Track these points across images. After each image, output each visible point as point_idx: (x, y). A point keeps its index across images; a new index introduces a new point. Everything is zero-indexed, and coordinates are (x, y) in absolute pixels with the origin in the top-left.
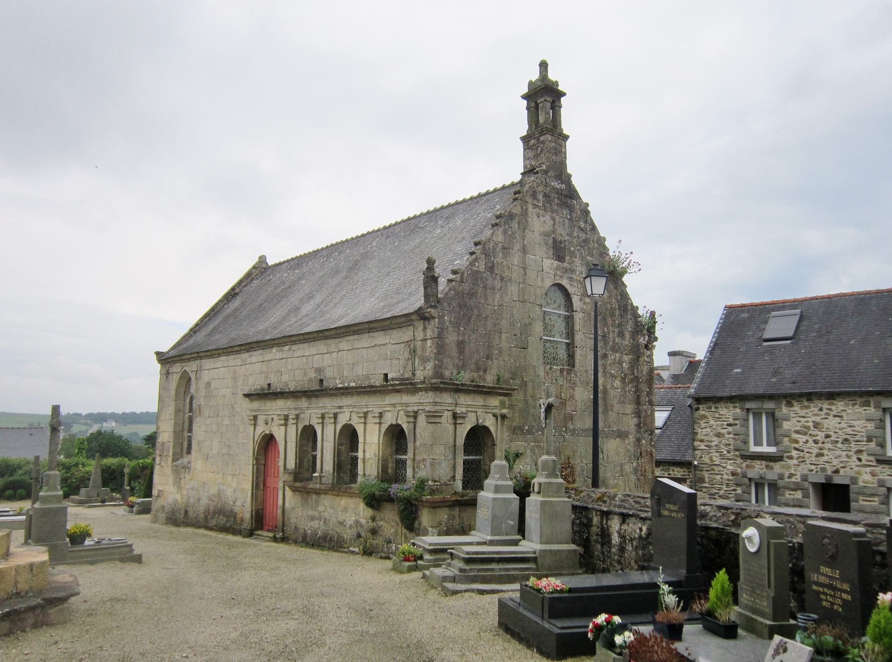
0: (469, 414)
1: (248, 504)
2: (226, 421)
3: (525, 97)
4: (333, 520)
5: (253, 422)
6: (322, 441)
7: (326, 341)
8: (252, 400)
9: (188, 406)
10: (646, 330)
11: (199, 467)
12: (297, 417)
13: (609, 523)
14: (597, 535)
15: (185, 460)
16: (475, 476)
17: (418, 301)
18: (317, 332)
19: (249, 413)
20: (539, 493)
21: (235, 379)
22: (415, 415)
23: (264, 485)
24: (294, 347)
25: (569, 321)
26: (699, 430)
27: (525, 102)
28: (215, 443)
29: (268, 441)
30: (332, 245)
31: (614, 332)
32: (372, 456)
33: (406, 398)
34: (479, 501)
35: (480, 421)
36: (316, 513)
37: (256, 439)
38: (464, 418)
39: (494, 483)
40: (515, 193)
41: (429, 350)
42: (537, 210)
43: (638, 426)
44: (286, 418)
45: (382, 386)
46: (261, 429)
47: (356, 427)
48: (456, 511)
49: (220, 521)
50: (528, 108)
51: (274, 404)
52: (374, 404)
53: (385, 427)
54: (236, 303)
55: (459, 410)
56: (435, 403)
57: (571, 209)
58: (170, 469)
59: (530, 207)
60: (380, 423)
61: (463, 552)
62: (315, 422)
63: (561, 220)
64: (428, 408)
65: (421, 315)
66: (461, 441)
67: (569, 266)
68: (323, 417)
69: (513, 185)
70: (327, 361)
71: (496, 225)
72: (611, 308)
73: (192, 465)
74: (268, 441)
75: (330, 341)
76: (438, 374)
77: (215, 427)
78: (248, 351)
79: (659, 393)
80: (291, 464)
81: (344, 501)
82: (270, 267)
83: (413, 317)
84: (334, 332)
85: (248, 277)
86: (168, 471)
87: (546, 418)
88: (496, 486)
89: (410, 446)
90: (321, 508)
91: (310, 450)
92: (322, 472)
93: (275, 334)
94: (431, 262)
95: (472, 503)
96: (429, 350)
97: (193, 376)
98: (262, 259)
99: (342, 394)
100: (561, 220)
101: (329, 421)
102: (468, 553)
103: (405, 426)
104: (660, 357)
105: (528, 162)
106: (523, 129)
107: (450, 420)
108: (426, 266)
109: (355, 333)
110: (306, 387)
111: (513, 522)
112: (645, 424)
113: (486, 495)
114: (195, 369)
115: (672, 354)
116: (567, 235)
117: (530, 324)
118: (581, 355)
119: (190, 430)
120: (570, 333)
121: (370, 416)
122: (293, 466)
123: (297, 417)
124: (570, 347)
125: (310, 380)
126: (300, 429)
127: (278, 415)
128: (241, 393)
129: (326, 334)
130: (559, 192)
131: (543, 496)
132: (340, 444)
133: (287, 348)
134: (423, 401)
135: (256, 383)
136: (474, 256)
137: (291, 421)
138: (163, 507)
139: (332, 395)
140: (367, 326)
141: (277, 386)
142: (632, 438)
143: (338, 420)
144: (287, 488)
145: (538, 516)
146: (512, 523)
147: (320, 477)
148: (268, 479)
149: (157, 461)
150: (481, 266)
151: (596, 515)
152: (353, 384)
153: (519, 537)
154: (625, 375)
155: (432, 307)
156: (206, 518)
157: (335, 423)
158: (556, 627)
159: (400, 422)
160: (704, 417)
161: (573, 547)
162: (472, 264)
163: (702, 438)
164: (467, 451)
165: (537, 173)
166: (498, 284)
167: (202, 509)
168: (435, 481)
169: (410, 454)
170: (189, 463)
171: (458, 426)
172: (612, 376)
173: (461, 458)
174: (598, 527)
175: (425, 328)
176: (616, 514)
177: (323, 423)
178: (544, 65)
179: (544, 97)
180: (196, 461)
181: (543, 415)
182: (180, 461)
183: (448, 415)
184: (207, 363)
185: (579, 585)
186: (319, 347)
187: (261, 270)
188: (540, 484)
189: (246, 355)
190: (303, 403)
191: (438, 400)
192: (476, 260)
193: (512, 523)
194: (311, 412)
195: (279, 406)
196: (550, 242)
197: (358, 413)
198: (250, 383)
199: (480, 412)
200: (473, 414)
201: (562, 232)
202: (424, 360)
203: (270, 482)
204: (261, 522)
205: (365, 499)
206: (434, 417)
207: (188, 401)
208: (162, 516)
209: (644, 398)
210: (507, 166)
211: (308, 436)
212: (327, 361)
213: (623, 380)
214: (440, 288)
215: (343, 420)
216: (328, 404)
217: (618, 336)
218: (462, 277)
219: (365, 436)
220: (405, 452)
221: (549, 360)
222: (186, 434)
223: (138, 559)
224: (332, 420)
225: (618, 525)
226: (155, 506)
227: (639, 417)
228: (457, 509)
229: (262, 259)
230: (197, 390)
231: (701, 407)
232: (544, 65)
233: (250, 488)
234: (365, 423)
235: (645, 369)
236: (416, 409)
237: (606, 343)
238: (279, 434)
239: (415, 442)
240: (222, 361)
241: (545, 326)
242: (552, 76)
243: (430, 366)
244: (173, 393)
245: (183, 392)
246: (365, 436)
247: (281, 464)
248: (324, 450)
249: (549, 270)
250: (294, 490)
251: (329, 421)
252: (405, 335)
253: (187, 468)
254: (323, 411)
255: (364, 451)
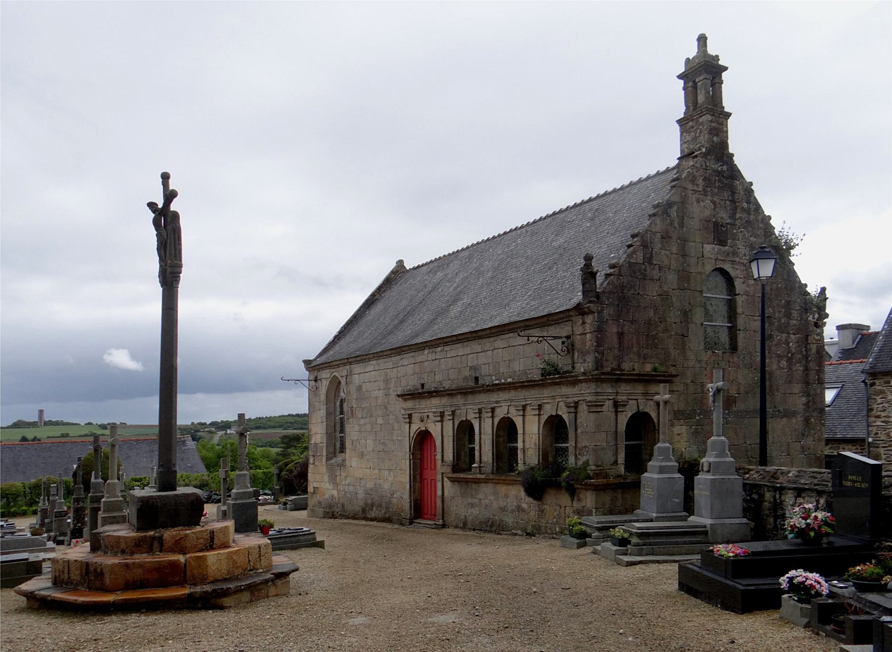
0: (630, 402)
1: (406, 496)
2: (380, 421)
3: (728, 115)
4: (495, 505)
5: (408, 420)
6: (480, 434)
7: (480, 341)
8: (405, 400)
9: (338, 409)
10: (816, 307)
11: (354, 464)
12: (453, 413)
13: (783, 498)
14: (769, 510)
15: (339, 459)
16: (637, 461)
17: (578, 297)
18: (471, 332)
19: (403, 412)
20: (708, 471)
21: (387, 381)
22: (576, 404)
23: (421, 477)
24: (447, 348)
25: (731, 306)
26: (876, 406)
27: (681, 83)
28: (370, 442)
29: (423, 439)
30: (473, 245)
31: (779, 312)
32: (532, 446)
33: (565, 390)
34: (643, 482)
35: (641, 408)
36: (476, 501)
37: (412, 435)
38: (625, 405)
39: (658, 464)
40: (673, 181)
41: (588, 344)
42: (697, 195)
43: (807, 405)
44: (442, 415)
45: (541, 380)
46: (416, 426)
47: (514, 419)
48: (619, 495)
49: (370, 513)
50: (684, 89)
51: (428, 402)
52: (532, 396)
53: (544, 418)
54: (378, 307)
55: (620, 398)
56: (597, 394)
57: (733, 191)
58: (324, 467)
59: (690, 193)
60: (539, 415)
61: (634, 527)
62: (472, 417)
63: (722, 203)
64: (589, 399)
65: (579, 310)
66: (622, 427)
67: (731, 249)
68: (480, 412)
69: (668, 170)
70: (482, 359)
71: (654, 215)
72: (777, 288)
73: (348, 463)
74: (423, 439)
75: (485, 340)
76: (598, 364)
77: (368, 427)
78: (399, 354)
79: (829, 371)
80: (449, 456)
81: (503, 489)
82: (408, 271)
83: (571, 313)
84: (489, 332)
85: (388, 282)
86: (323, 469)
87: (714, 401)
88: (660, 466)
89: (571, 435)
90: (481, 496)
91: (467, 443)
92: (481, 462)
93: (426, 337)
94: (588, 258)
95: (636, 486)
96: (588, 344)
97: (343, 381)
98: (400, 263)
99: (499, 390)
100: (722, 203)
101: (487, 415)
102: (639, 528)
103: (565, 417)
104: (830, 332)
105: (686, 145)
106: (680, 111)
107: (612, 409)
108: (583, 262)
109: (510, 331)
110: (462, 384)
111: (679, 500)
112: (814, 403)
113: (651, 476)
114: (345, 374)
115: (840, 328)
116: (729, 217)
117: (691, 310)
118: (745, 338)
119: (342, 430)
120: (732, 315)
121: (528, 408)
122: (451, 458)
123: (453, 413)
124: (733, 332)
125: (466, 378)
126: (457, 423)
127: (434, 412)
128: (393, 394)
129: (480, 334)
130: (719, 173)
131: (713, 475)
132: (498, 436)
133: (439, 349)
134: (585, 392)
135: (412, 383)
136: (632, 248)
137: (447, 418)
138: (319, 502)
139: (489, 391)
140: (523, 324)
141: (430, 386)
142: (800, 418)
143: (496, 414)
144: (446, 479)
145: (708, 493)
146: (677, 500)
147: (480, 467)
148: (425, 472)
149: (311, 461)
150: (639, 257)
151: (769, 491)
152: (509, 380)
153: (685, 514)
154: (793, 354)
155: (591, 302)
156: (364, 510)
157: (493, 417)
158: (741, 584)
159: (560, 413)
160: (882, 392)
161: (744, 520)
162: (630, 256)
163: (879, 413)
164: (628, 438)
165: (696, 156)
166: (656, 273)
167: (361, 503)
168: (598, 466)
169: (571, 444)
170: (344, 460)
171: (619, 414)
172: (779, 356)
173: (622, 444)
174: (770, 502)
175: (584, 323)
176: (790, 489)
177: (480, 417)
178: (702, 40)
179: (703, 76)
180: (351, 459)
181: (711, 399)
182: (334, 460)
183: (608, 405)
184: (357, 368)
185: (761, 549)
186: (475, 346)
187: (399, 272)
188: (710, 464)
189: (398, 358)
190: (459, 400)
191: (599, 390)
192: (634, 252)
193: (677, 500)
194: (468, 410)
195: (435, 403)
196: (711, 225)
197: (516, 406)
198: (403, 384)
199: (635, 400)
200: (634, 402)
201: (724, 216)
202: (584, 354)
203: (428, 474)
204: (421, 509)
205: (523, 485)
206: (595, 407)
207: (338, 404)
208: (320, 511)
209: (813, 376)
210: (664, 151)
211: (465, 431)
212: (482, 359)
213: (790, 360)
214: (598, 283)
215: (500, 413)
216: (484, 399)
217: (785, 316)
218: (620, 271)
219: (524, 427)
220: (566, 440)
221: (710, 345)
222: (338, 435)
223: (321, 545)
224: (490, 415)
225: (793, 499)
226: (311, 503)
227: (808, 395)
228: (620, 491)
229: (400, 263)
230: (349, 394)
231: (877, 382)
232: (702, 40)
233: (408, 481)
234: (524, 416)
235: (814, 348)
236: (576, 399)
237: (771, 324)
238: (435, 429)
239: (576, 430)
240: (372, 365)
241: (707, 312)
242: (712, 50)
243: (590, 359)
244: (323, 397)
245: (333, 395)
246: (524, 427)
247: (439, 457)
248: (483, 443)
249: (709, 256)
250: (453, 480)
251: (487, 415)
252: (564, 330)
253: (342, 465)
254: (480, 407)
255: (524, 442)
